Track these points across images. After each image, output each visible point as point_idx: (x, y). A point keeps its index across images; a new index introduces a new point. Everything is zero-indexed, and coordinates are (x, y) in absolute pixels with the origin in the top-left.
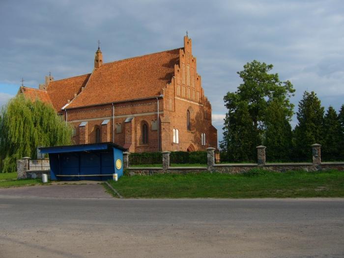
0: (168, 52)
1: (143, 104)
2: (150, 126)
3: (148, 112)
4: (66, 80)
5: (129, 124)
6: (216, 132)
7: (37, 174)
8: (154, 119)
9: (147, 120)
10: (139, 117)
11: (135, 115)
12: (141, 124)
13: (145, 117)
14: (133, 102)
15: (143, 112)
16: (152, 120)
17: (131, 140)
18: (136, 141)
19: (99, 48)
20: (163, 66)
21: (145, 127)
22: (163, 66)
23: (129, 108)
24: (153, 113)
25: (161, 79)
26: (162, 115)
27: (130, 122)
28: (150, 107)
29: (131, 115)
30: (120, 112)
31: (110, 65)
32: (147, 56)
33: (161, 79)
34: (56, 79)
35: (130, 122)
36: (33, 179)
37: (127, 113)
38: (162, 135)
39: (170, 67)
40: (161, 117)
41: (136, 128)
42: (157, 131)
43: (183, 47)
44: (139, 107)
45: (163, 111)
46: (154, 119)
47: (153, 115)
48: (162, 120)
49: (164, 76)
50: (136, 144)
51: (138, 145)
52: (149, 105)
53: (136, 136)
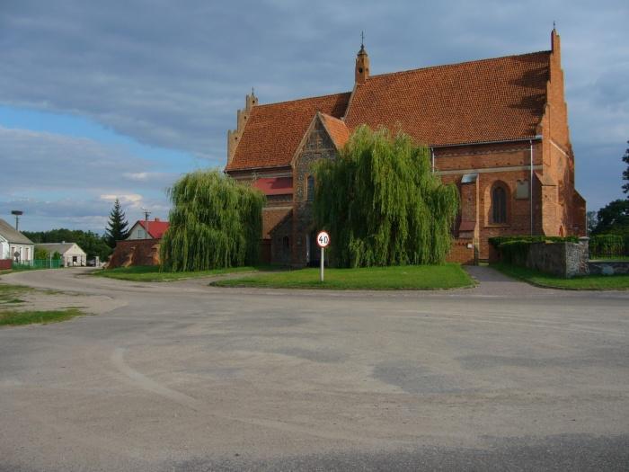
0: (514, 58)
1: (498, 150)
2: (512, 191)
3: (509, 165)
4: (292, 103)
5: (471, 187)
6: (584, 206)
7: (614, 267)
8: (522, 179)
9: (507, 182)
10: (488, 174)
11: (480, 171)
12: (492, 188)
13: (504, 174)
14: (475, 148)
15: (497, 166)
16: (519, 181)
17: (474, 216)
18: (482, 216)
19: (362, 47)
20: (510, 82)
21: (500, 191)
22: (510, 82)
23: (467, 158)
24: (520, 168)
25: (513, 106)
26: (540, 171)
27: (473, 182)
28: (518, 156)
29: (472, 171)
30: (446, 164)
31: (388, 79)
32: (470, 64)
33: (513, 106)
34: (260, 103)
35: (473, 182)
36: (607, 275)
37: (462, 166)
38: (543, 208)
39: (526, 86)
40: (538, 175)
41: (482, 194)
42: (528, 199)
43: (548, 48)
44: (489, 157)
45: (541, 164)
46: (522, 179)
47: (520, 172)
48: (542, 179)
49: (518, 101)
50: (482, 222)
51: (486, 224)
52: (512, 153)
53: (482, 208)
